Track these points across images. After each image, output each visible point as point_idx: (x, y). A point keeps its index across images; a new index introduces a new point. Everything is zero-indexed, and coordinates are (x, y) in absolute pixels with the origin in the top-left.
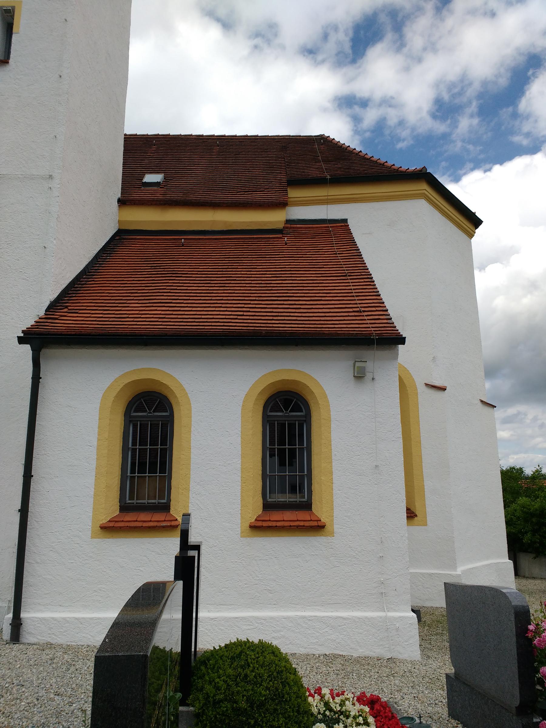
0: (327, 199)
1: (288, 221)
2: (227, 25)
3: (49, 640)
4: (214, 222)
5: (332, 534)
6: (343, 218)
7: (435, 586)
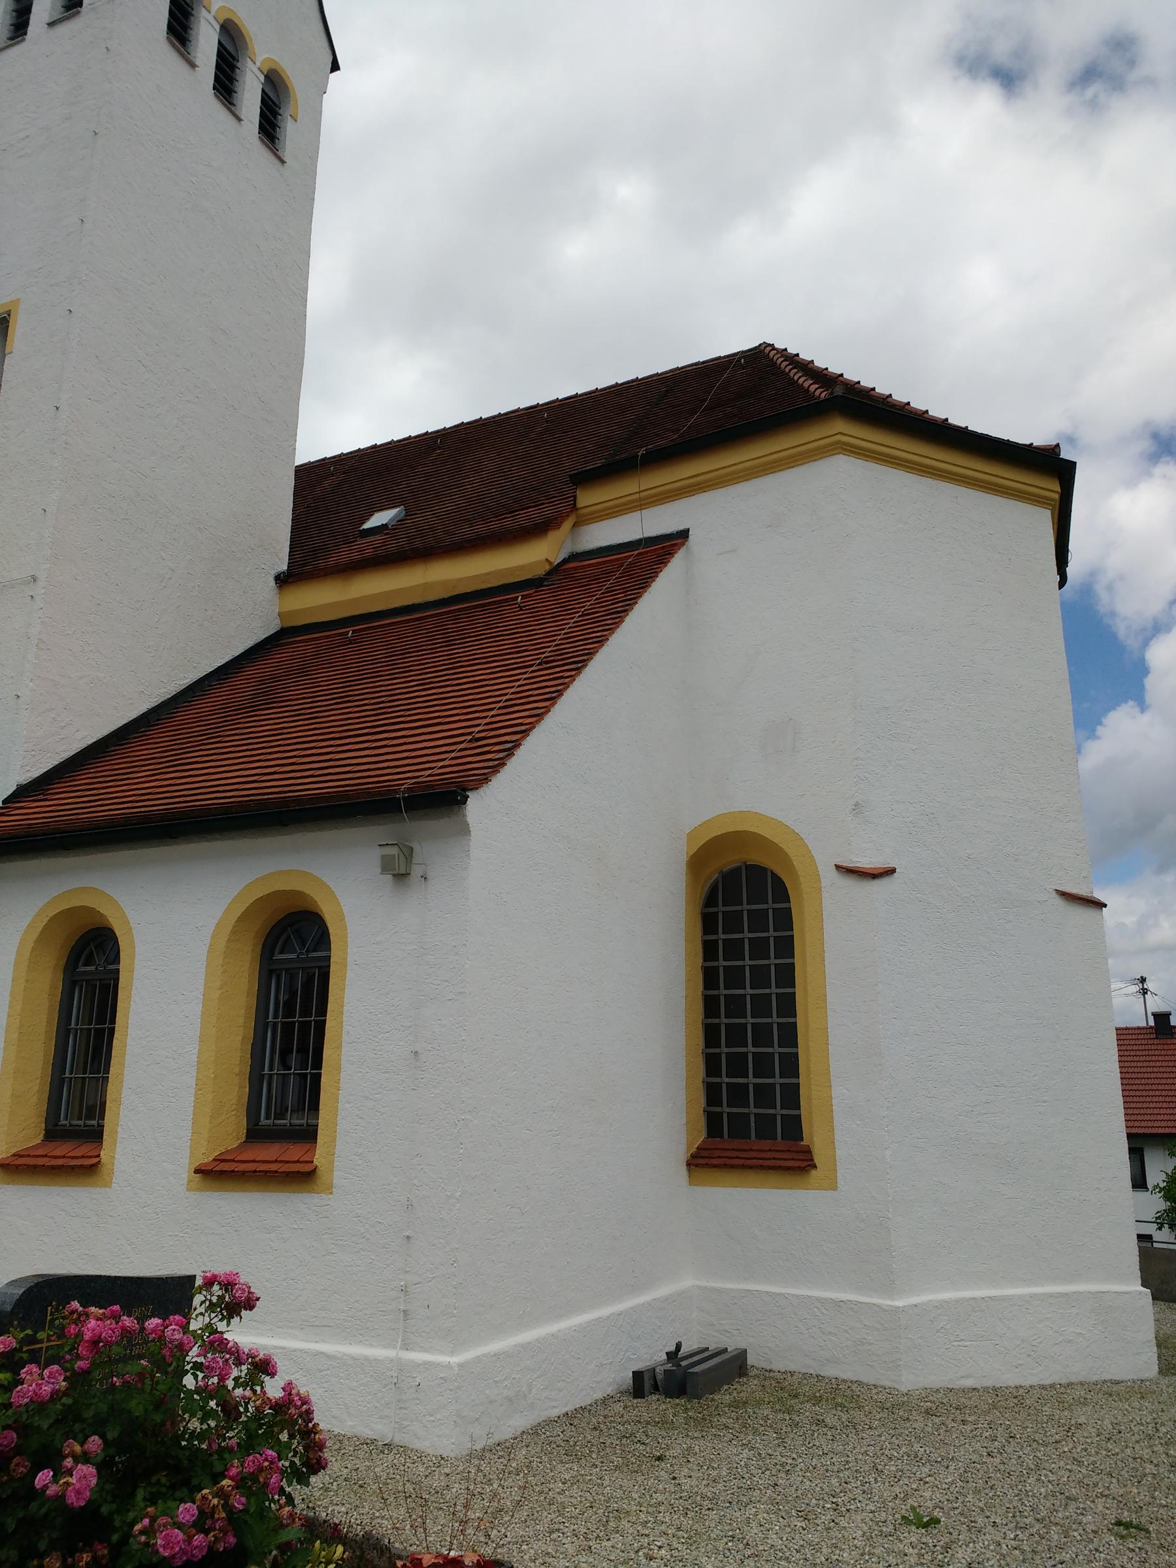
0: (640, 499)
1: (574, 557)
2: (1009, 78)
5: (329, 1189)
6: (682, 528)
7: (846, 1331)
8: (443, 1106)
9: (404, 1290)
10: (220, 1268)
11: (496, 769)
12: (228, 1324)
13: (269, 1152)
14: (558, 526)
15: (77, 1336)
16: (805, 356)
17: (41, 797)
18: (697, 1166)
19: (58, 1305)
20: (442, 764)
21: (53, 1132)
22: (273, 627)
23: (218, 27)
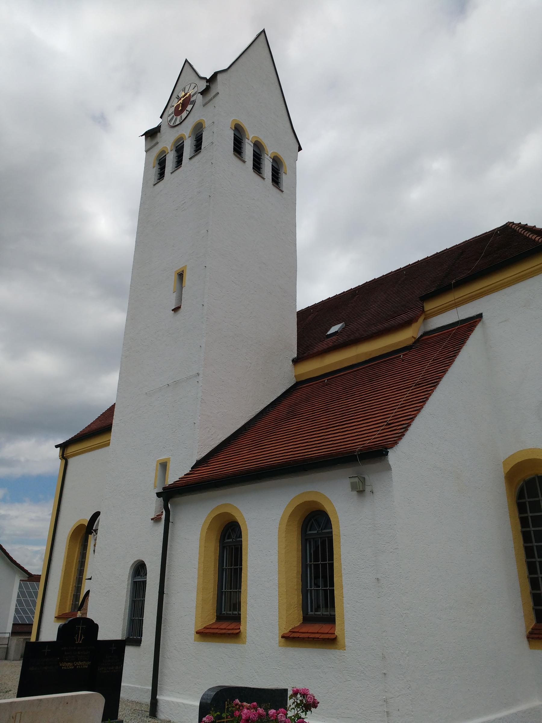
0: (455, 303)
1: (426, 334)
3: (170, 718)
4: (358, 356)
5: (343, 647)
6: (478, 313)
8: (394, 606)
9: (385, 701)
10: (300, 686)
11: (400, 437)
12: (306, 714)
13: (314, 628)
14: (416, 321)
15: (239, 716)
16: (530, 224)
17: (206, 465)
18: (533, 638)
19: (230, 701)
20: (374, 437)
21: (220, 618)
22: (293, 382)
23: (252, 145)
